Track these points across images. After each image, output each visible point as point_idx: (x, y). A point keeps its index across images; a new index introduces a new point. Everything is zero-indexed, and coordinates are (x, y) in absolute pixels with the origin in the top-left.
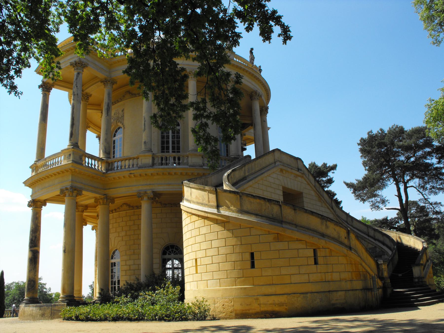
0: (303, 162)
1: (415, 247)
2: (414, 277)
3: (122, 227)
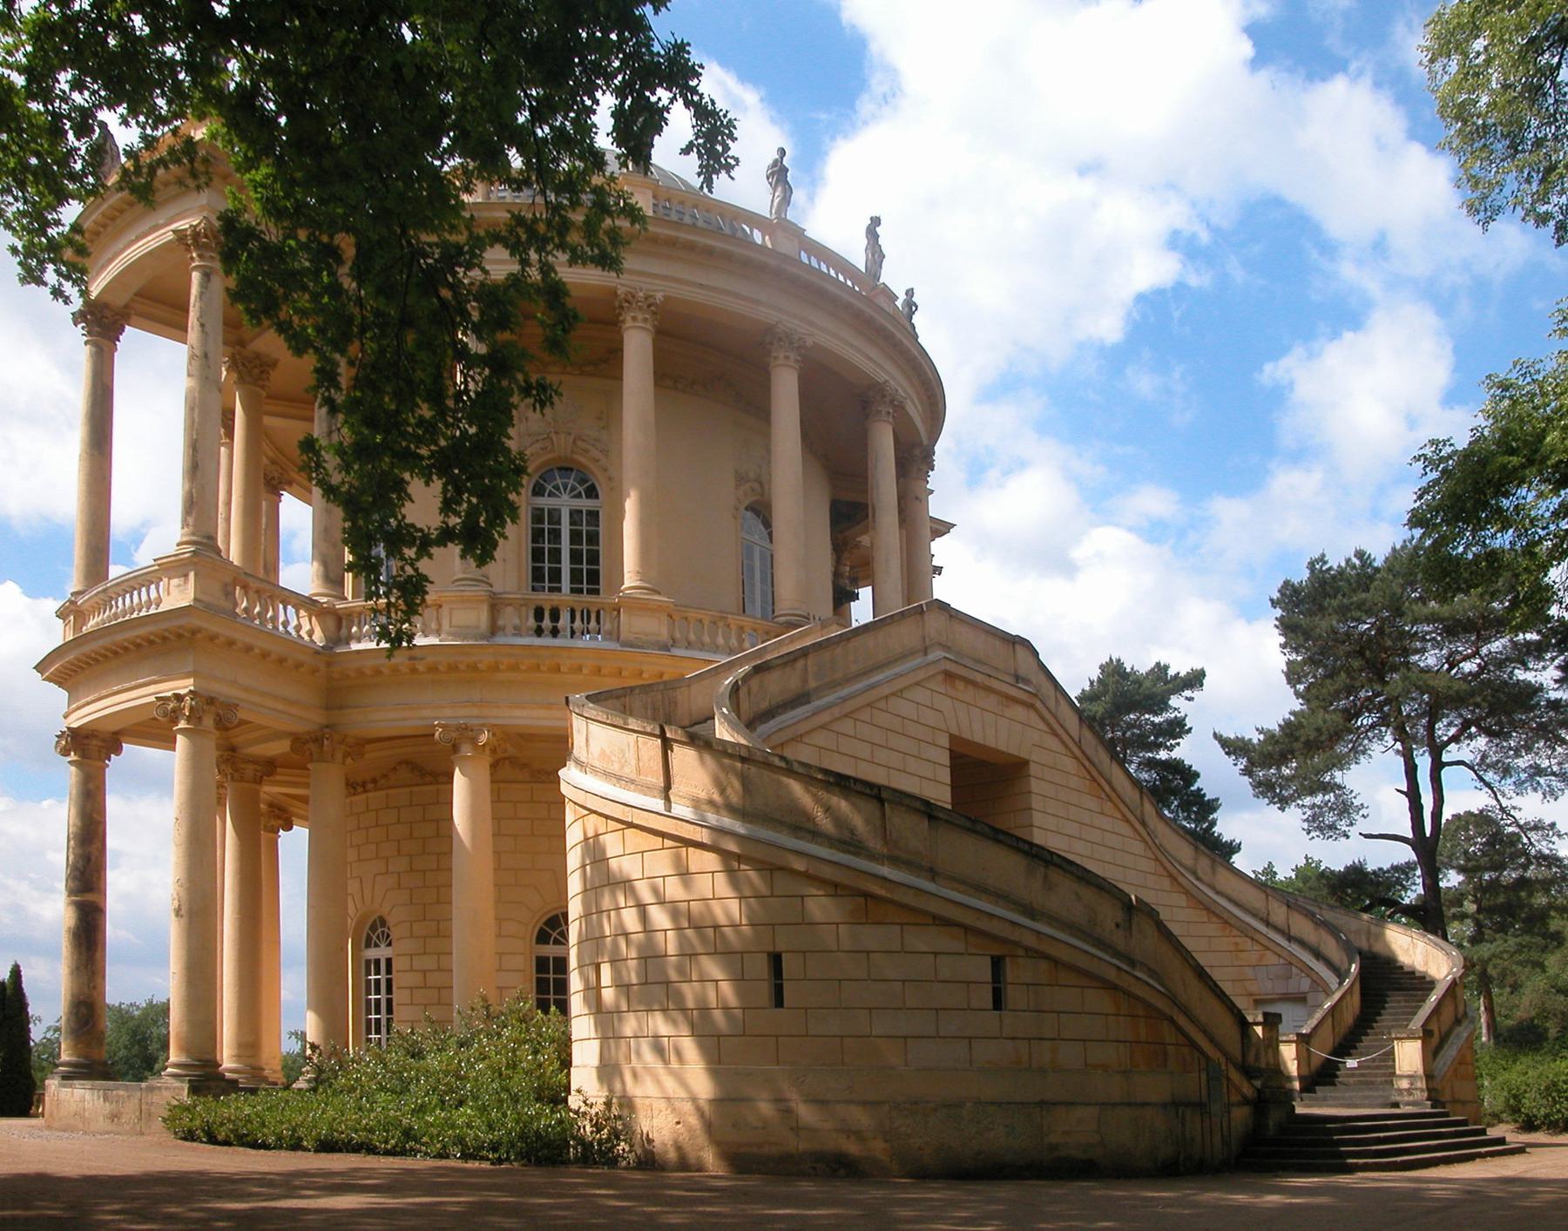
1: (1426, 972)
2: (1398, 1072)
3: (399, 841)
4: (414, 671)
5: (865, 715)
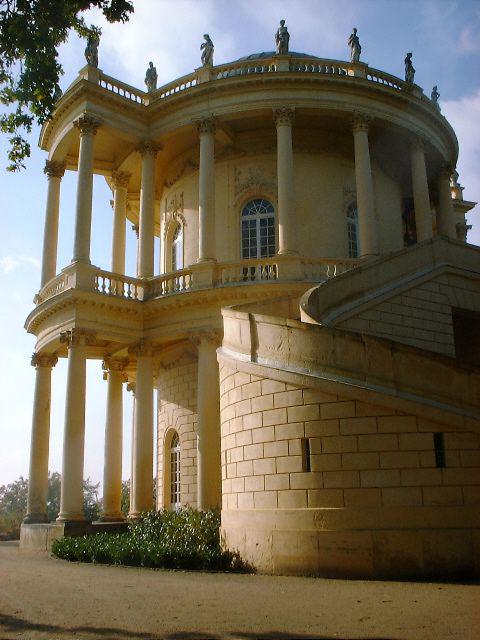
4: (180, 306)
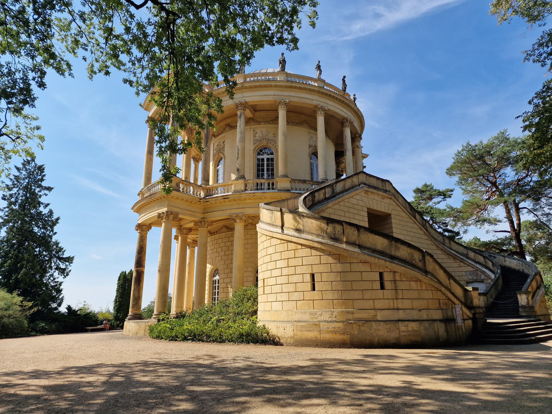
0: (391, 184)
5: (342, 204)
